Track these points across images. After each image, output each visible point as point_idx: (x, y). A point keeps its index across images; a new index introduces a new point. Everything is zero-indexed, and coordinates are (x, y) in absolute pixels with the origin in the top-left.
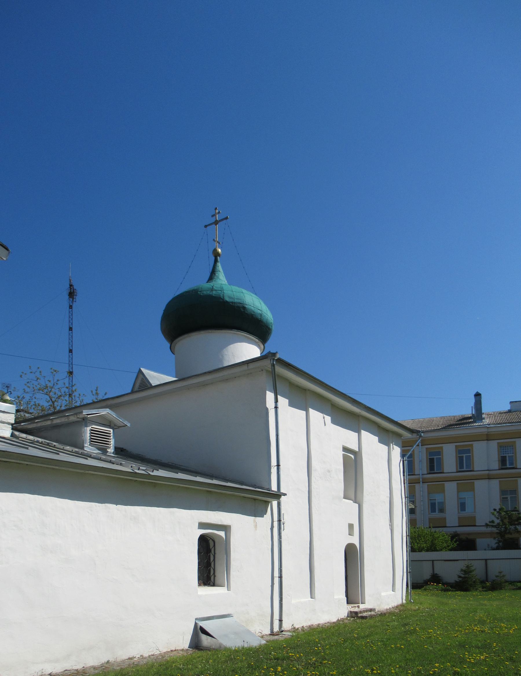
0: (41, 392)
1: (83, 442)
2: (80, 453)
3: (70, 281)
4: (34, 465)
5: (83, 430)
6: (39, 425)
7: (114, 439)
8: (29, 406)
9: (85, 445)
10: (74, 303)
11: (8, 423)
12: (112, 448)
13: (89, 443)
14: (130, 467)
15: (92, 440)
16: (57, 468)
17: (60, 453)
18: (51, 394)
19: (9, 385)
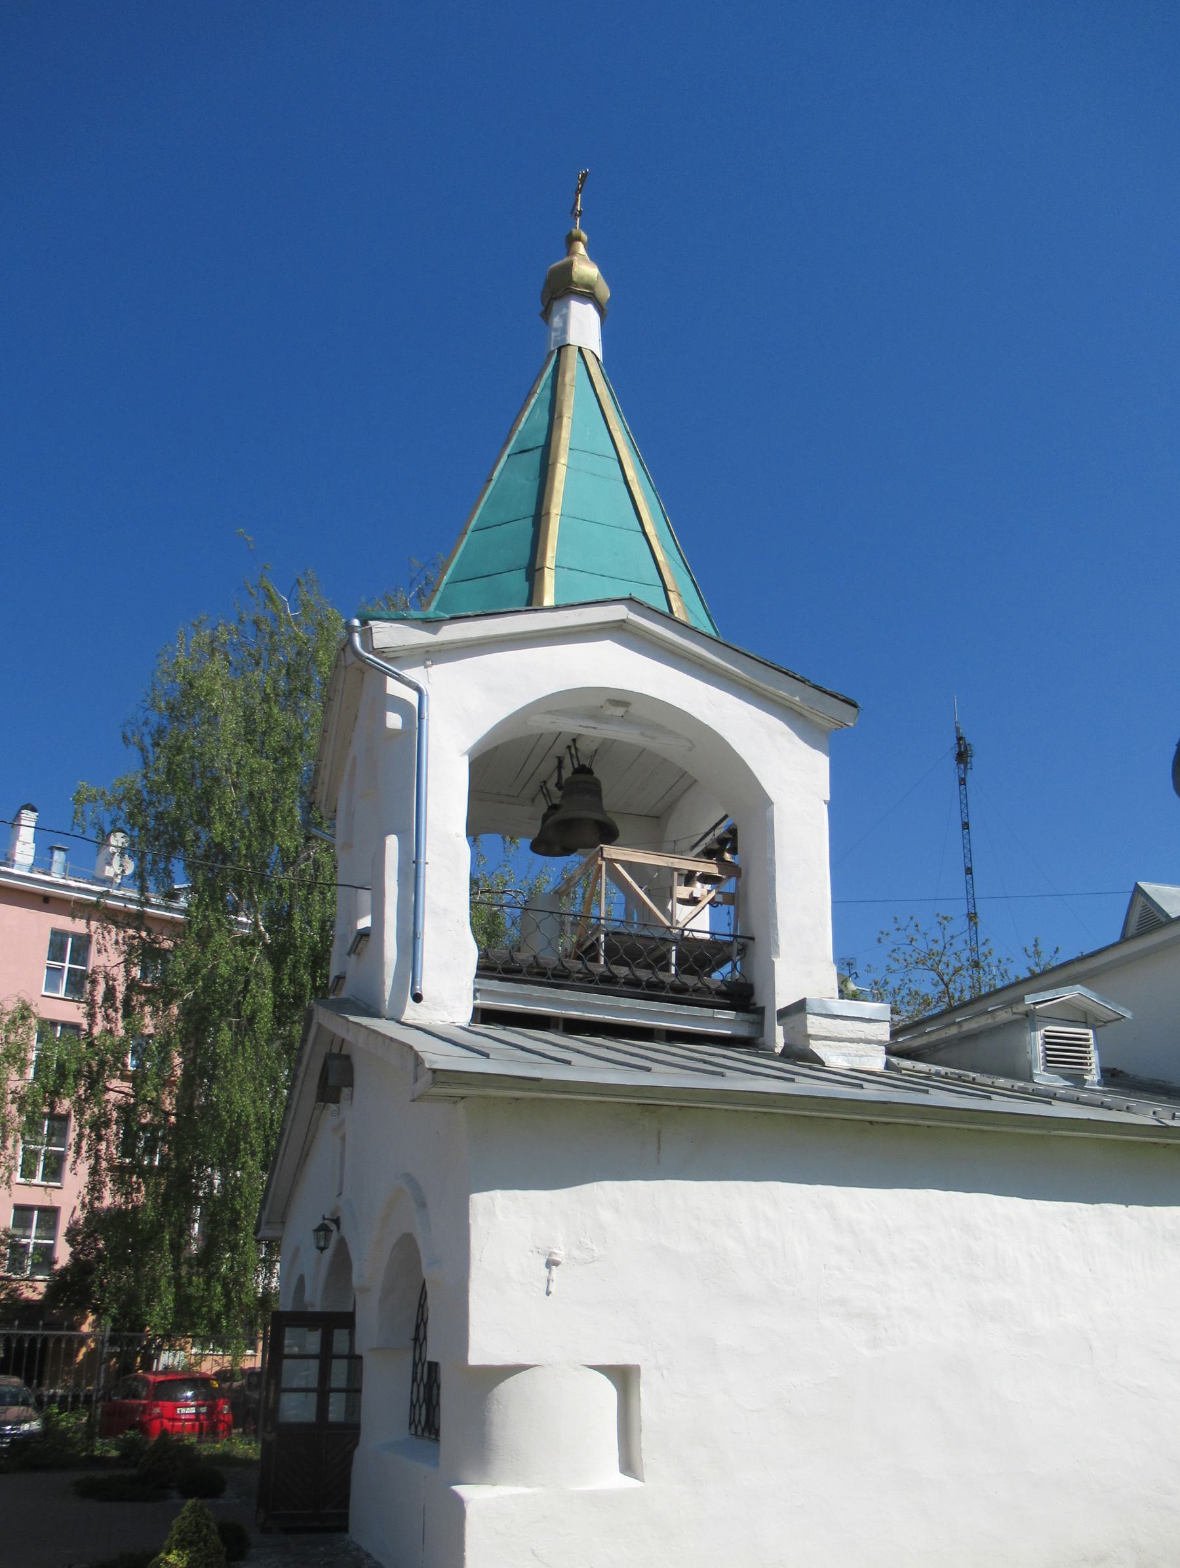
0: (920, 966)
1: (1030, 1065)
2: (1031, 1091)
3: (957, 729)
4: (777, 1113)
5: (1028, 1038)
6: (934, 1038)
7: (1097, 1052)
8: (899, 998)
9: (1035, 1072)
10: (969, 771)
11: (879, 1043)
12: (1094, 1072)
13: (1042, 1067)
14: (1151, 1114)
15: (1048, 1058)
16: (991, 1128)
17: (993, 1096)
18: (941, 967)
19: (852, 961)
